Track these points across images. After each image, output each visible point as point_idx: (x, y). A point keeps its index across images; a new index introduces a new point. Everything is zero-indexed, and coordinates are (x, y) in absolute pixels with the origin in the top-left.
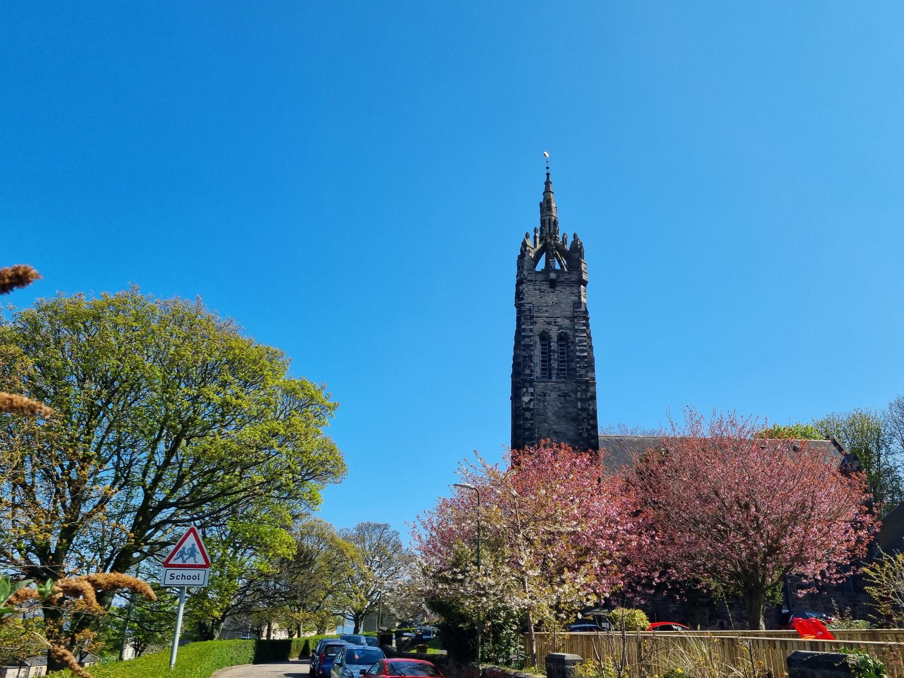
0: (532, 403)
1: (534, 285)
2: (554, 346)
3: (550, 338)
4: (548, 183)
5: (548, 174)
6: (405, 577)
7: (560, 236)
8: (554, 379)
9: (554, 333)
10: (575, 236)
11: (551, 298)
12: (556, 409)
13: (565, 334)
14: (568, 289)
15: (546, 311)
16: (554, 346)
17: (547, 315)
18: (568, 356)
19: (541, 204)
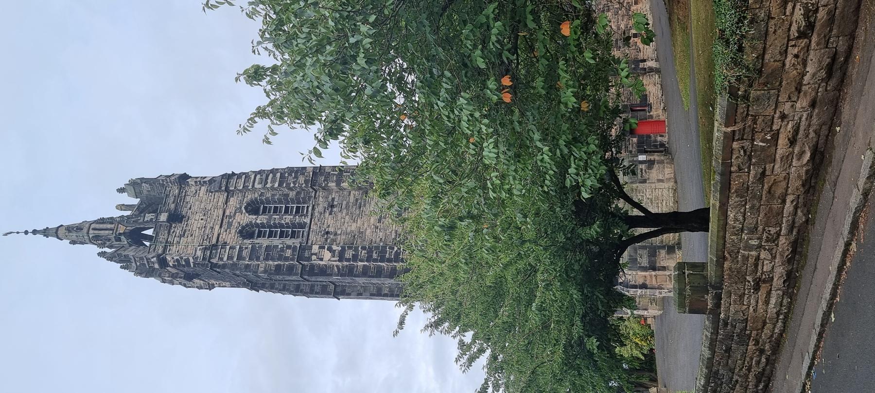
0: (334, 247)
1: (172, 244)
2: (262, 219)
3: (250, 225)
4: (46, 232)
5: (35, 232)
6: (517, 189)
7: (117, 214)
8: (307, 220)
9: (245, 219)
10: (121, 190)
11: (196, 222)
12: (347, 218)
13: (248, 204)
14: (188, 199)
15: (212, 228)
16: (262, 219)
17: (217, 227)
18: (280, 202)
19: (73, 242)
